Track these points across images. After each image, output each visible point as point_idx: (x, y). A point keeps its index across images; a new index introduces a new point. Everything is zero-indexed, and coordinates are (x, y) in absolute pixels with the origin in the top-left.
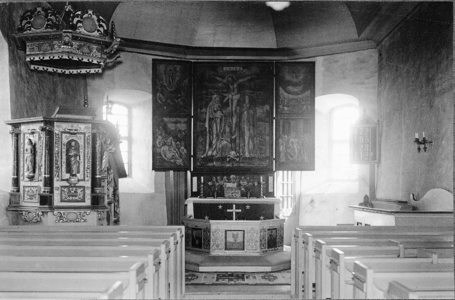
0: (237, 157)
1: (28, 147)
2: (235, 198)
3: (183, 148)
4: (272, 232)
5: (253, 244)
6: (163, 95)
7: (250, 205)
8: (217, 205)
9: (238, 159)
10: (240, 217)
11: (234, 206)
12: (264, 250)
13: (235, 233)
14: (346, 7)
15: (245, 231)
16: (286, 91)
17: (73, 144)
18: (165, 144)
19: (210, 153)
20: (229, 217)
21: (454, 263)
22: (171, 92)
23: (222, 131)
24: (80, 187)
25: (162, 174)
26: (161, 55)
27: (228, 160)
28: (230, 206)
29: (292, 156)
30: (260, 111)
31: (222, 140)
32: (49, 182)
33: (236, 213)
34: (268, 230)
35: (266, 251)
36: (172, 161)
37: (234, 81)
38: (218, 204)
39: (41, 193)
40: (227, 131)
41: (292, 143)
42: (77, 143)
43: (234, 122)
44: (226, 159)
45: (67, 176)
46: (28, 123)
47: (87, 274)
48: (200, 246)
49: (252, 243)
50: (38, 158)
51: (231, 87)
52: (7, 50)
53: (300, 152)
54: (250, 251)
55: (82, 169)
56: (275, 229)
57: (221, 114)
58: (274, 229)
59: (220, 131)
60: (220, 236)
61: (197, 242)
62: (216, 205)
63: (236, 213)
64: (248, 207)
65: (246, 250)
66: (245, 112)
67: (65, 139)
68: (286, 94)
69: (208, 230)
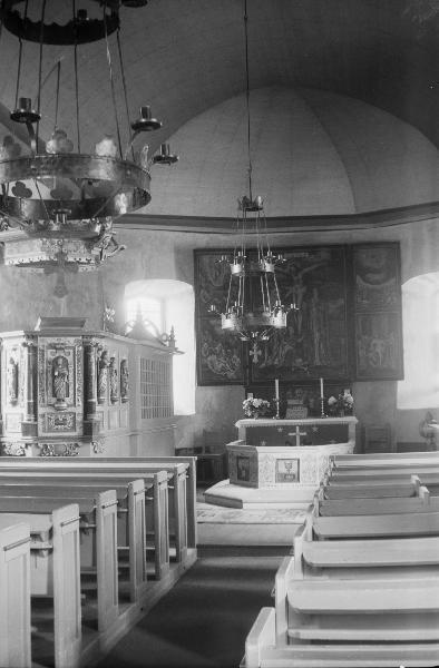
1: (11, 367)
3: (235, 356)
6: (208, 292)
7: (317, 426)
10: (305, 442)
13: (288, 462)
14: (68, 288)
16: (364, 280)
17: (60, 361)
18: (212, 353)
19: (270, 362)
20: (290, 443)
22: (219, 289)
24: (70, 413)
25: (211, 392)
26: (202, 239)
28: (292, 428)
29: (375, 363)
30: (333, 307)
32: (33, 409)
33: (301, 437)
36: (222, 373)
37: (298, 270)
38: (278, 427)
39: (25, 421)
41: (375, 345)
42: (65, 360)
43: (300, 322)
45: (54, 400)
46: (10, 338)
47: (372, 532)
48: (247, 479)
50: (20, 380)
51: (295, 278)
53: (384, 354)
55: (71, 392)
61: (244, 474)
63: (301, 437)
64: (315, 429)
66: (314, 309)
67: (50, 355)
68: (362, 282)
69: (254, 459)
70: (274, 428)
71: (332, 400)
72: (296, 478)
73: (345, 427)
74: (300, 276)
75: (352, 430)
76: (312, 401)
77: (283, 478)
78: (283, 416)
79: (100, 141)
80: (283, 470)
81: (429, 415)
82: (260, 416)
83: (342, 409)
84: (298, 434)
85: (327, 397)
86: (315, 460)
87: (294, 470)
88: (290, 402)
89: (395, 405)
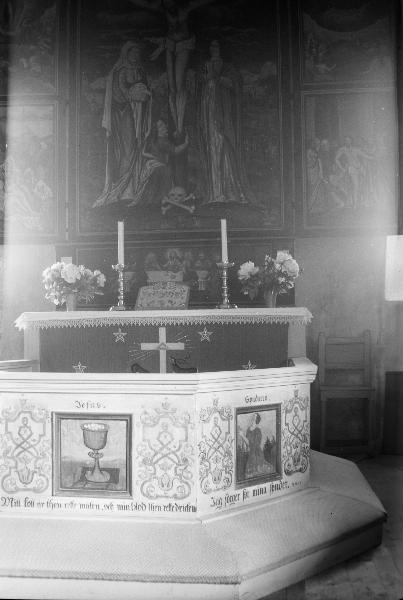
0: (189, 203)
2: (168, 308)
4: (258, 419)
5: (171, 473)
7: (210, 326)
10: (180, 364)
11: (162, 332)
12: (222, 494)
13: (94, 426)
15: (136, 421)
20: (144, 364)
21: (5, 105)
23: (147, 135)
27: (164, 210)
28: (150, 332)
31: (148, 159)
33: (170, 353)
34: (241, 411)
35: (231, 499)
38: (115, 328)
40: (160, 135)
51: (172, 20)
52: (387, 276)
56: (277, 407)
57: (146, 91)
58: (268, 408)
59: (143, 135)
60: (35, 436)
63: (170, 353)
64: (205, 335)
65: (138, 496)
66: (211, 84)
70: (108, 330)
71: (247, 268)
72: (117, 480)
73: (280, 330)
74: (183, 15)
75: (297, 341)
76: (202, 274)
77: (78, 479)
78: (131, 304)
79: (246, 261)
80: (80, 454)
81: (393, 377)
82: (81, 306)
83: (267, 289)
84: (163, 345)
85: (237, 258)
86: (187, 425)
87: (113, 454)
88: (152, 276)
89: (381, 295)
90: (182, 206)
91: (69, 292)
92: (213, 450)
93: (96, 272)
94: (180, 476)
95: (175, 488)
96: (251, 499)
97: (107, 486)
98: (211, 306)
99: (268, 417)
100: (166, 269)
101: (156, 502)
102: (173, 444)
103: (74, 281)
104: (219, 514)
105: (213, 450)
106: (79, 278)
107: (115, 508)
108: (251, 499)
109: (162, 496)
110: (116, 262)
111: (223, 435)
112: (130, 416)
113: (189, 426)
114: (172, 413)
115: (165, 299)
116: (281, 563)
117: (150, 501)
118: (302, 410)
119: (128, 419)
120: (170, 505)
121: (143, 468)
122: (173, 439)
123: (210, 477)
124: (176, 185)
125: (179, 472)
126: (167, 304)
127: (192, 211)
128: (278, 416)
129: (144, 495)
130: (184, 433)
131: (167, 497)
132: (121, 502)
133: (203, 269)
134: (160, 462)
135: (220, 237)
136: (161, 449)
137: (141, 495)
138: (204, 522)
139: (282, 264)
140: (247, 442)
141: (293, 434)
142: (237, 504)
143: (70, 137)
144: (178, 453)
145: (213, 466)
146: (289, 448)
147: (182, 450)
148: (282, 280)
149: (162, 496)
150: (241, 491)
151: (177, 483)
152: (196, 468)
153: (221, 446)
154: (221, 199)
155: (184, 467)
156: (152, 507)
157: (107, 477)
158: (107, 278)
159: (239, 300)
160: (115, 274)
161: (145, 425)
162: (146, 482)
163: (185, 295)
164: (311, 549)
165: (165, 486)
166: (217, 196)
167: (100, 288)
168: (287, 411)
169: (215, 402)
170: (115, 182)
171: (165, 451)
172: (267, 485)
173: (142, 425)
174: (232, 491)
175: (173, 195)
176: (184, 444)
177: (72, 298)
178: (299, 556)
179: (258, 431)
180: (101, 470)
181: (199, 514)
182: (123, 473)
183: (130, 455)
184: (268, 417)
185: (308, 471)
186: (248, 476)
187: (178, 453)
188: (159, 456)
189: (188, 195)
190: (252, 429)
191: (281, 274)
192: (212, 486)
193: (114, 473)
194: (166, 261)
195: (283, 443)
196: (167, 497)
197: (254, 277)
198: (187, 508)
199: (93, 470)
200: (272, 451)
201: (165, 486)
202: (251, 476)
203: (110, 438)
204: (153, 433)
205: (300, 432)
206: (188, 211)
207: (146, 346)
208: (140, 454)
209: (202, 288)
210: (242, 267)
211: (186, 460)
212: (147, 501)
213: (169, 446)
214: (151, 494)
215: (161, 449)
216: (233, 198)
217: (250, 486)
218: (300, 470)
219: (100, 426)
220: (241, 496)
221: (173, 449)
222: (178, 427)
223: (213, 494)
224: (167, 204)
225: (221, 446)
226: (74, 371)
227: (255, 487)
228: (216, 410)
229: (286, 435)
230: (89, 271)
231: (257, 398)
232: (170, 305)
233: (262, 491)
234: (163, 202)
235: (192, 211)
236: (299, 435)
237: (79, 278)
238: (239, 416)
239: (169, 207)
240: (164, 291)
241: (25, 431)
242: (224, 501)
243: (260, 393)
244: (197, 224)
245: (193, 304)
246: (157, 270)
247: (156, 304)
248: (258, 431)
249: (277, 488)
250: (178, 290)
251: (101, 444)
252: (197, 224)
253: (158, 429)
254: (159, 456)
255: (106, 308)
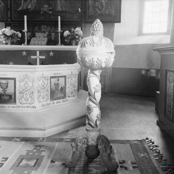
0: (50, 10)
2: (40, 45)
4: (58, 80)
5: (28, 96)
8: (21, 51)
9: (51, 12)
10: (43, 63)
11: (38, 53)
12: (45, 103)
20: (32, 63)
27: (42, 12)
28: (34, 53)
29: (100, 10)
33: (40, 59)
35: (48, 104)
38: (23, 51)
44: (40, 13)
49: (26, 94)
54: (23, 105)
56: (65, 77)
62: (20, 51)
64: (51, 54)
65: (18, 104)
71: (66, 33)
76: (53, 34)
78: (28, 43)
82: (12, 43)
88: (37, 34)
90: (47, 11)
91: (8, 39)
92: (42, 89)
93: (18, 32)
94: (31, 97)
95: (29, 101)
96: (56, 104)
97: (8, 100)
98: (55, 45)
99: (62, 80)
100: (42, 32)
101: (23, 105)
102: (29, 87)
103: (10, 35)
104: (44, 109)
105: (42, 89)
106: (11, 34)
107: (11, 107)
108: (56, 104)
109: (25, 104)
110: (24, 29)
111: (46, 85)
112: (15, 78)
113: (34, 82)
114: (28, 78)
115: (39, 42)
116: (60, 124)
117: (22, 105)
118: (74, 78)
119: (14, 79)
120: (28, 106)
121: (20, 95)
122: (29, 86)
123: (41, 98)
124: (46, 4)
125: (30, 96)
126: (40, 44)
127: (51, 13)
128: (65, 79)
129: (20, 103)
130: (32, 84)
131: (27, 104)
132: (12, 105)
133: (53, 33)
134: (25, 93)
135: (58, 22)
136: (25, 89)
137: (19, 103)
138: (38, 111)
139: (77, 31)
140: (55, 87)
141: (70, 85)
142: (51, 106)
143: (81, 3)
144: (30, 90)
145: (42, 94)
146: (69, 89)
147: (31, 89)
148: (77, 37)
149: (25, 104)
150: (52, 102)
151: (30, 99)
152: (36, 95)
153: (45, 88)
154: (60, 9)
155: (32, 94)
156: (22, 107)
157: (8, 98)
158: (22, 34)
159: (64, 43)
160: (24, 33)
161: (20, 81)
162: (20, 99)
163: (46, 41)
164: (72, 120)
165: (27, 100)
166: (59, 8)
167: (19, 38)
168: (68, 78)
169: (43, 75)
170: (25, 2)
171: (26, 89)
172: (61, 100)
173: (19, 81)
174: (49, 102)
175: (45, 7)
176: (32, 87)
177: (9, 41)
178: (67, 122)
179: (58, 84)
180: (6, 95)
181: (37, 109)
182: (13, 97)
183: (15, 91)
184: (62, 80)
185: (76, 96)
186: (55, 97)
187: (30, 90)
188: (24, 91)
189: (49, 8)
190: (56, 83)
191: (77, 35)
192: (42, 100)
193: (10, 96)
194: (42, 30)
195: (67, 88)
196: (27, 104)
197: (68, 36)
198: (34, 107)
199: (4, 95)
200: (63, 90)
201: (27, 100)
202: (56, 97)
203: (9, 85)
204: (22, 84)
205: (73, 84)
206: (50, 13)
207: (33, 57)
208: (18, 90)
209: (53, 39)
210: (65, 32)
211: (33, 92)
212: (21, 105)
213: (28, 88)
214: (22, 103)
215: (25, 89)
216: (64, 10)
217: (55, 100)
218: (73, 96)
219: (6, 82)
220: (52, 104)
221: (29, 89)
222: (30, 82)
223: (42, 103)
224: (43, 10)
225: (45, 88)
226: (9, 64)
227: (57, 101)
228: (43, 77)
229: (68, 85)
230: (15, 32)
231: (58, 74)
232: (41, 44)
233: (59, 102)
234: (41, 10)
235: (51, 13)
236: (73, 85)
237: (11, 34)
238: (51, 79)
239: (43, 12)
240: (39, 39)
241: (26, 85)
242: (46, 105)
243: (59, 72)
244: (52, 17)
245: (48, 44)
246: (39, 32)
247: (36, 44)
248: (58, 84)
249: (65, 101)
250: (44, 39)
251: (6, 87)
252: (52, 17)
253: (24, 82)
254: (24, 91)
255: (21, 44)
